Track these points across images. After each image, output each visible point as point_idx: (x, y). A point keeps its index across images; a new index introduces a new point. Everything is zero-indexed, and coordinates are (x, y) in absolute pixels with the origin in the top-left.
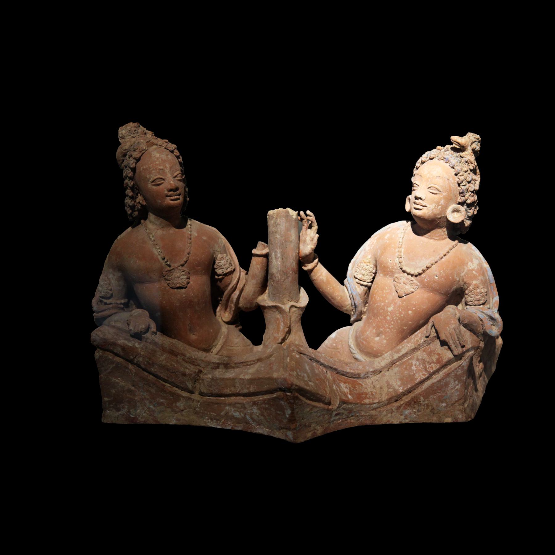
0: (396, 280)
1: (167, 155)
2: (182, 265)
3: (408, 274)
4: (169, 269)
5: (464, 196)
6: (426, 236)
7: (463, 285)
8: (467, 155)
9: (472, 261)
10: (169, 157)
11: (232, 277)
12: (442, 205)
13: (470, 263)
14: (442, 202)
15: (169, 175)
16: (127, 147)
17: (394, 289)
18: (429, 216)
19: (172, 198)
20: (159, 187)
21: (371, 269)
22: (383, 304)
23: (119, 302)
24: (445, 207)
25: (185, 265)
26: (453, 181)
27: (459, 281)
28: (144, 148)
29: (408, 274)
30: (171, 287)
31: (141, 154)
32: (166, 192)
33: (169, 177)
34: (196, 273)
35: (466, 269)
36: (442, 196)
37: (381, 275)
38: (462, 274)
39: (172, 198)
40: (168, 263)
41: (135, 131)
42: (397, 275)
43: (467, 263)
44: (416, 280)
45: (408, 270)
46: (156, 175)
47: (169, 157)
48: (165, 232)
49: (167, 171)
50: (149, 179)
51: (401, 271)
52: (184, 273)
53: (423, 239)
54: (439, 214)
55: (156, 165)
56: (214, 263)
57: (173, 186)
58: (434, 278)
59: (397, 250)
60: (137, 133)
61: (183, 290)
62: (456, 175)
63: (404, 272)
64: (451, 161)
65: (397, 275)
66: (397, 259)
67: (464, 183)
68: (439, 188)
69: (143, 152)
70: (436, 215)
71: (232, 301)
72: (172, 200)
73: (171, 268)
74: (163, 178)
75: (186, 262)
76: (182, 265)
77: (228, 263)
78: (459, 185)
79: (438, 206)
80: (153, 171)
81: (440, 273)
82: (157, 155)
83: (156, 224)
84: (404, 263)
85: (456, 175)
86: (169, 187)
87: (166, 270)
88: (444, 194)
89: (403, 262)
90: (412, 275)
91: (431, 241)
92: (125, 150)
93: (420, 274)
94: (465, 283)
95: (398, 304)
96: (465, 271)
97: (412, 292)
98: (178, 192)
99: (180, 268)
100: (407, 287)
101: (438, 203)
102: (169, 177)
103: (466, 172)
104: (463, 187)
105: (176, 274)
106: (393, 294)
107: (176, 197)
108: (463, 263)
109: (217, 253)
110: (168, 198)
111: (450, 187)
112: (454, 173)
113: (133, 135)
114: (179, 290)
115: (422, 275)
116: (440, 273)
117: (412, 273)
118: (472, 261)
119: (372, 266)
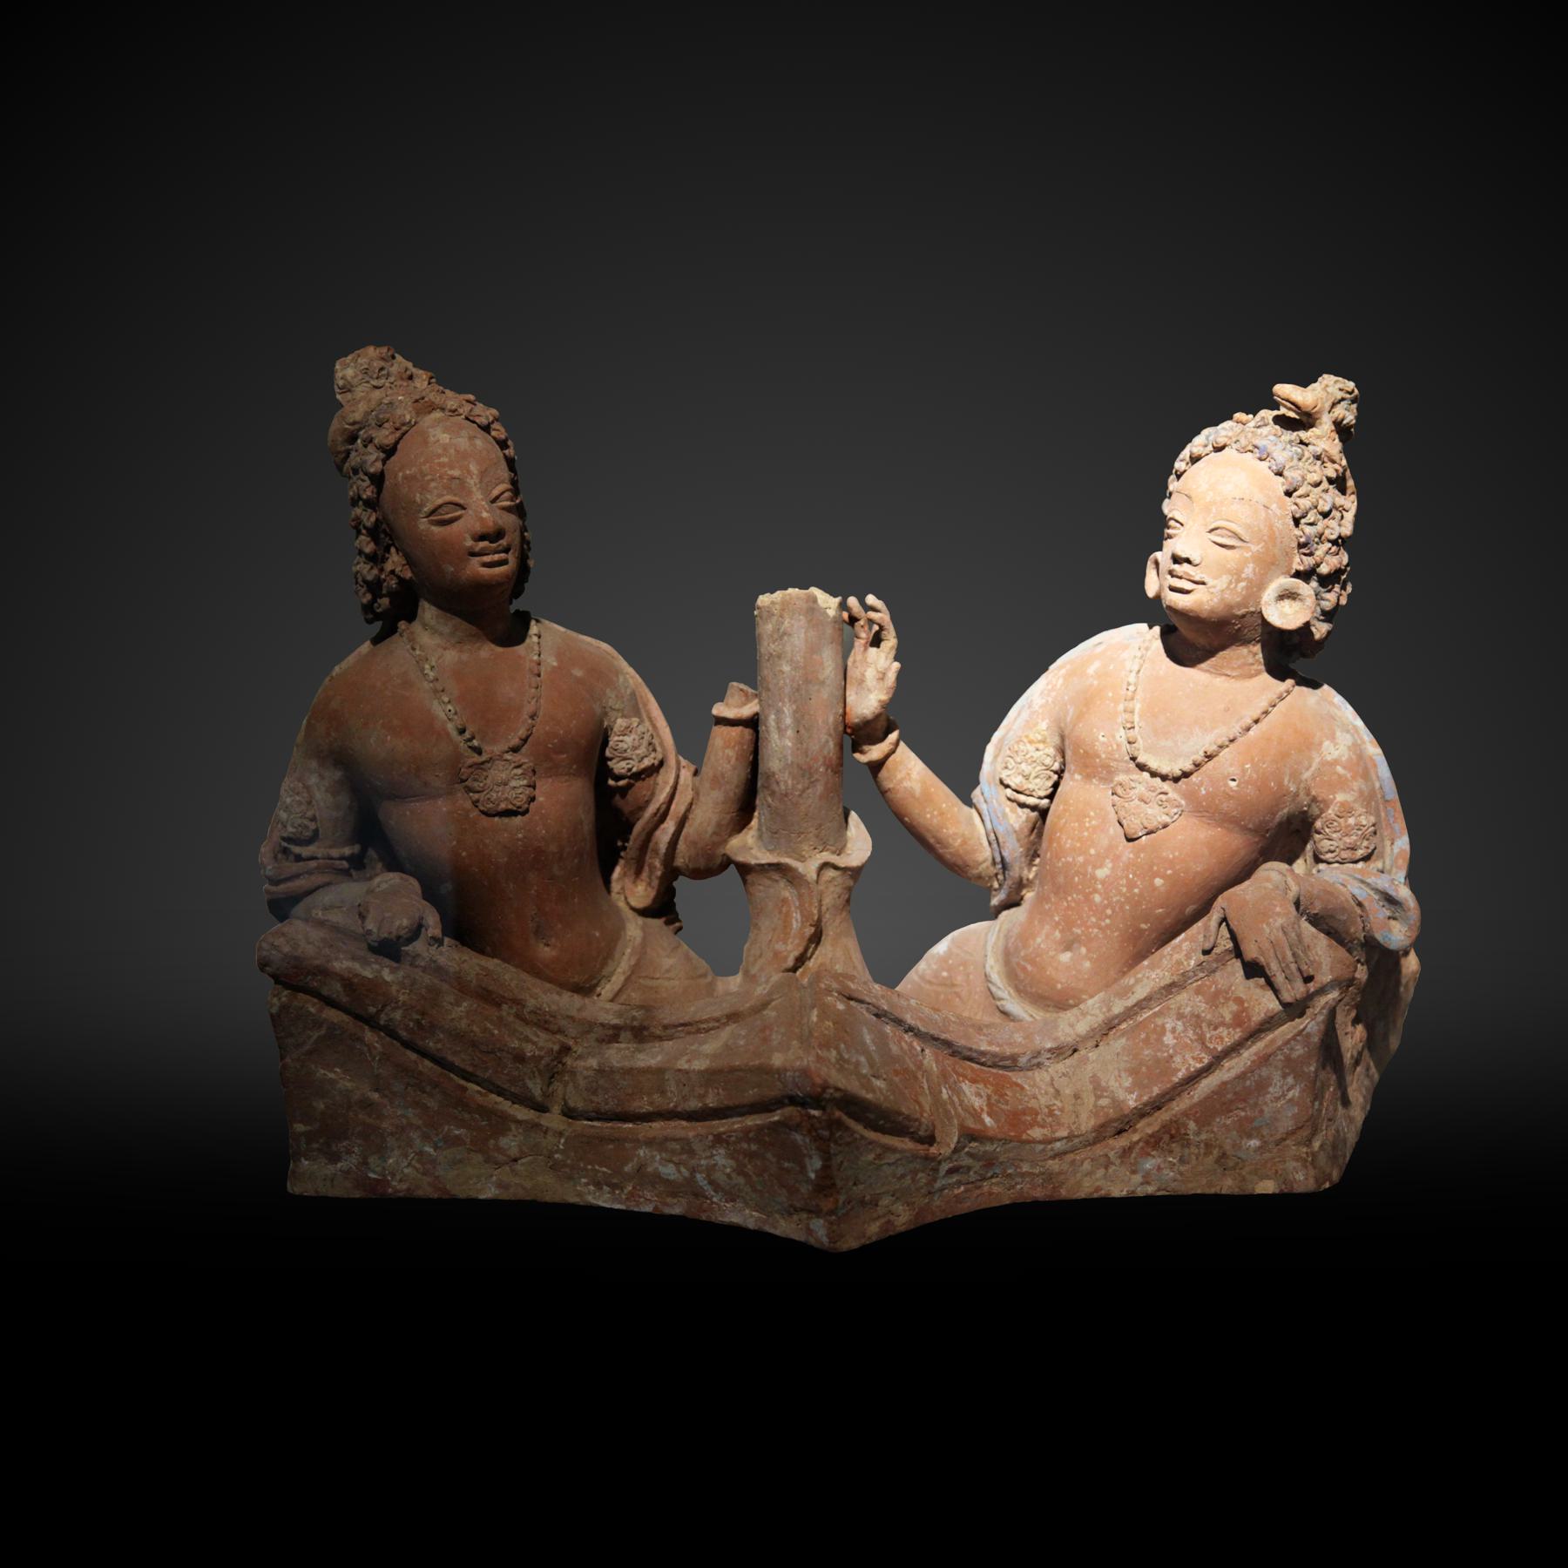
0: (1119, 791)
1: (471, 438)
2: (515, 750)
3: (1154, 774)
4: (477, 759)
5: (1311, 554)
6: (1203, 665)
7: (1309, 806)
8: (1318, 437)
9: (1333, 738)
10: (478, 442)
11: (656, 784)
12: (1249, 580)
13: (1326, 743)
14: (1249, 571)
15: (478, 495)
16: (357, 416)
17: (1113, 817)
18: (1212, 611)
19: (487, 559)
20: (448, 528)
21: (1048, 761)
22: (1081, 859)
23: (335, 853)
24: (1258, 586)
25: (523, 750)
26: (1278, 512)
27: (1297, 795)
28: (408, 418)
29: (1154, 774)
30: (483, 812)
31: (398, 434)
32: (469, 543)
33: (477, 499)
34: (554, 771)
35: (1317, 760)
36: (1248, 555)
37: (1077, 777)
38: (1307, 775)
39: (487, 559)
40: (475, 743)
41: (382, 369)
42: (1121, 778)
43: (1320, 744)
44: (1175, 790)
45: (1153, 764)
46: (440, 496)
47: (478, 442)
48: (465, 657)
49: (472, 482)
50: (422, 505)
51: (1132, 765)
52: (519, 771)
53: (1195, 676)
54: (1239, 605)
55: (442, 465)
56: (605, 743)
57: (490, 527)
58: (1226, 785)
59: (1121, 707)
60: (388, 375)
61: (518, 820)
62: (1289, 494)
63: (1142, 767)
64: (1275, 455)
65: (1121, 778)
66: (1122, 732)
67: (1311, 517)
68: (1239, 530)
69: (403, 430)
70: (1231, 607)
71: (656, 851)
72: (485, 565)
73: (484, 757)
74: (462, 502)
75: (525, 741)
76: (515, 750)
77: (645, 742)
78: (1297, 522)
79: (1238, 581)
80: (433, 484)
81: (1244, 771)
83: (441, 634)
84: (1140, 744)
85: (1289, 494)
86: (478, 528)
87: (470, 762)
88: (1254, 548)
89: (1140, 740)
90: (1164, 778)
91: (1219, 681)
92: (354, 423)
93: (1186, 775)
94: (1314, 800)
95: (1124, 859)
96: (1315, 766)
97: (1165, 826)
98: (504, 542)
99: (508, 756)
100: (1150, 811)
101: (1237, 575)
102: (477, 499)
103: (1317, 485)
104: (1308, 530)
105: (498, 773)
106: (1111, 831)
107: (496, 557)
108: (1307, 744)
109: (613, 714)
110: (475, 560)
111: (1271, 527)
112: (1281, 490)
113: (375, 383)
114: (506, 820)
115: (1193, 778)
116: (1244, 771)
117: (1165, 770)
118: (1333, 736)
119: (1051, 751)
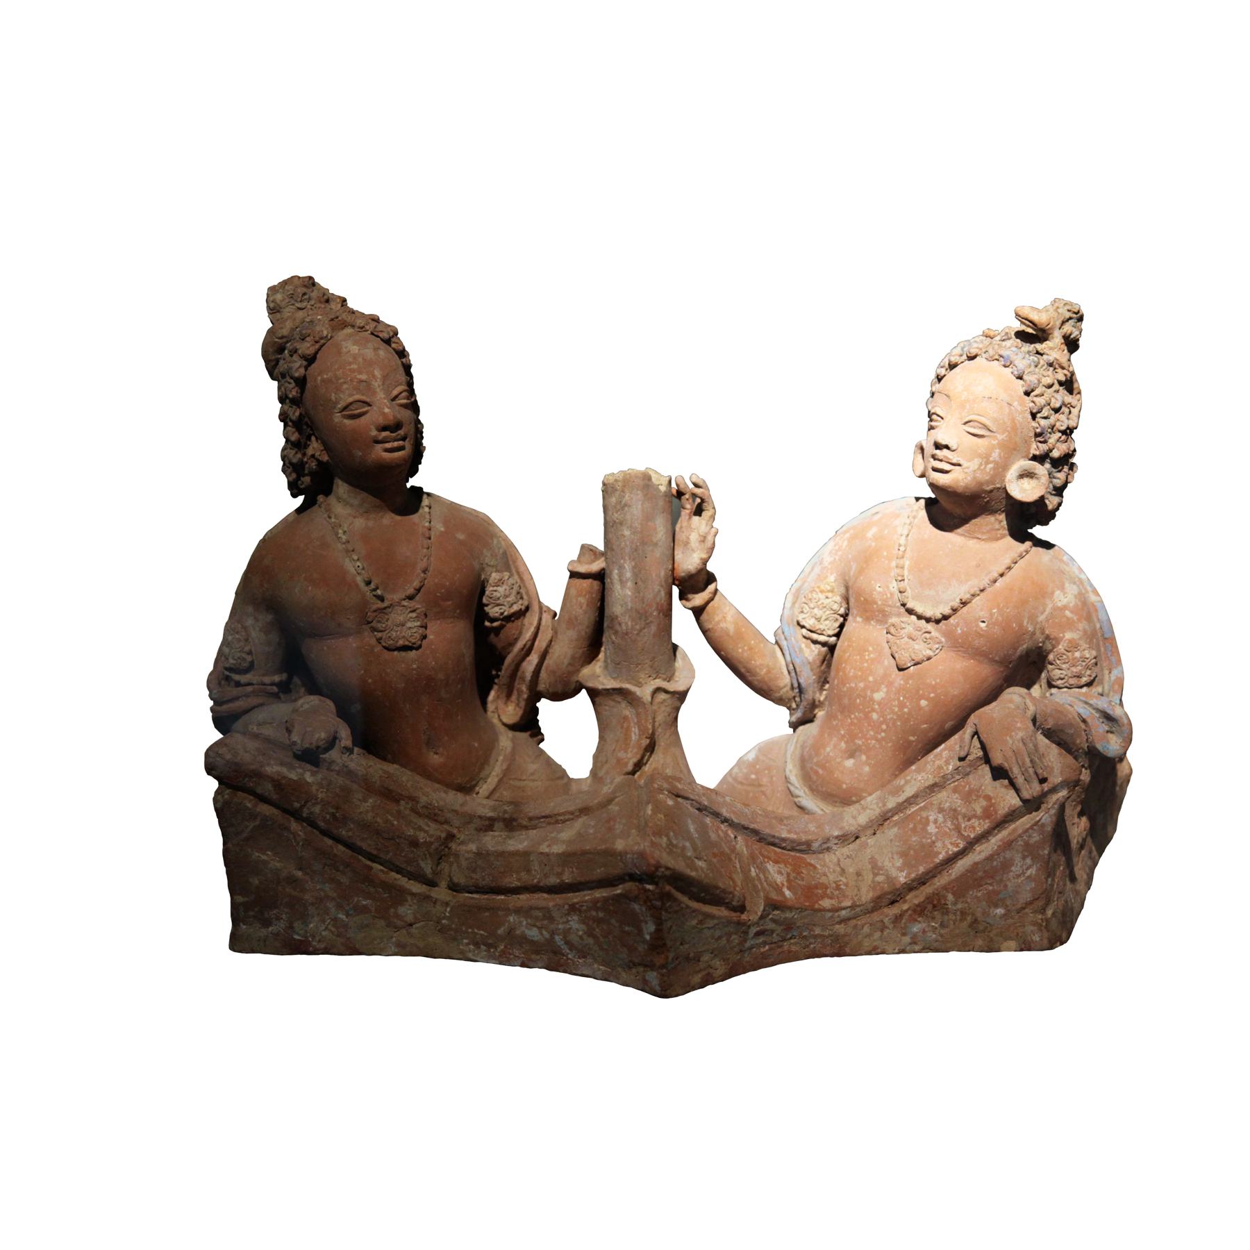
0: (892, 630)
1: (376, 349)
2: (411, 598)
3: (920, 617)
4: (380, 605)
5: (1045, 442)
6: (959, 530)
7: (1044, 642)
8: (1051, 349)
9: (1062, 588)
10: (381, 353)
11: (523, 625)
12: (996, 463)
13: (1057, 593)
14: (995, 455)
15: (381, 395)
17: (887, 651)
18: (966, 487)
19: (388, 445)
20: (357, 421)
21: (836, 607)
22: (862, 685)
23: (267, 680)
24: (1003, 467)
25: (417, 598)
26: (1019, 408)
27: (1034, 634)
28: (325, 333)
29: (920, 617)
30: (385, 648)
31: (317, 346)
32: (374, 433)
33: (381, 398)
34: (441, 615)
35: (1050, 606)
36: (995, 442)
37: (859, 619)
38: (1042, 618)
39: (388, 445)
40: (379, 592)
41: (304, 294)
42: (894, 620)
43: (1053, 593)
44: (937, 630)
45: (919, 609)
46: (351, 395)
47: (381, 353)
48: (371, 524)
49: (376, 384)
50: (336, 403)
51: (902, 610)
52: (414, 615)
53: (953, 539)
54: (988, 483)
55: (352, 371)
56: (483, 592)
57: (391, 420)
58: (977, 626)
59: (894, 564)
60: (309, 299)
61: (413, 654)
62: (1027, 394)
63: (910, 612)
64: (1016, 363)
65: (894, 620)
66: (895, 584)
67: (1045, 412)
68: (988, 423)
69: (321, 343)
70: (981, 484)
71: (523, 679)
72: (387, 450)
73: (386, 604)
74: (368, 400)
75: (418, 590)
76: (411, 598)
77: (514, 592)
78: (1034, 416)
79: (987, 463)
80: (345, 386)
81: (992, 615)
82: (355, 349)
83: (352, 506)
84: (909, 593)
85: (1027, 394)
86: (381, 421)
87: (374, 607)
88: (1000, 437)
89: (909, 590)
90: (928, 620)
91: (972, 543)
92: (282, 337)
93: (945, 618)
94: (1048, 637)
95: (896, 685)
96: (1048, 610)
97: (929, 659)
98: (401, 432)
99: (405, 603)
100: (917, 647)
101: (986, 458)
103: (1050, 386)
104: (1043, 422)
105: (397, 616)
106: (886, 662)
107: (396, 444)
109: (488, 569)
110: (379, 447)
111: (1013, 420)
112: (1022, 390)
113: (299, 305)
114: (403, 654)
115: (951, 620)
116: (992, 615)
117: (928, 614)
119: (838, 599)
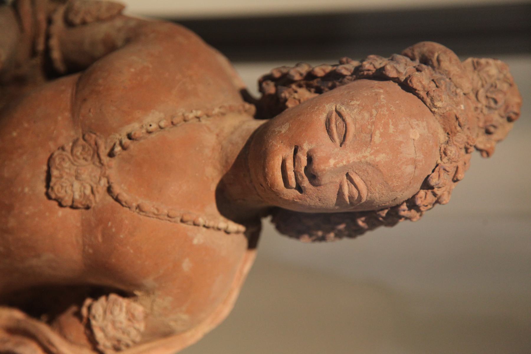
1: (414, 162)
2: (109, 190)
4: (104, 151)
10: (409, 169)
11: (82, 346)
15: (353, 158)
16: (445, 64)
19: (290, 164)
20: (323, 127)
23: (54, 42)
25: (109, 199)
28: (439, 104)
30: (52, 155)
31: (423, 94)
32: (306, 147)
33: (348, 157)
34: (88, 229)
39: (290, 164)
40: (118, 149)
41: (496, 102)
46: (355, 121)
47: (409, 169)
48: (207, 152)
49: (367, 154)
50: (348, 105)
52: (88, 192)
55: (386, 125)
56: (124, 294)
57: (319, 166)
60: (489, 108)
61: (41, 188)
69: (425, 99)
71: (18, 344)
72: (284, 162)
73: (105, 159)
74: (347, 142)
75: (117, 200)
76: (109, 190)
77: (119, 335)
80: (367, 115)
82: (415, 134)
83: (232, 133)
86: (318, 156)
87: (101, 142)
92: (438, 61)
98: (306, 183)
99: (104, 182)
102: (348, 157)
105: (89, 171)
107: (291, 173)
109: (147, 301)
110: (290, 153)
113: (482, 92)
114: (43, 177)
